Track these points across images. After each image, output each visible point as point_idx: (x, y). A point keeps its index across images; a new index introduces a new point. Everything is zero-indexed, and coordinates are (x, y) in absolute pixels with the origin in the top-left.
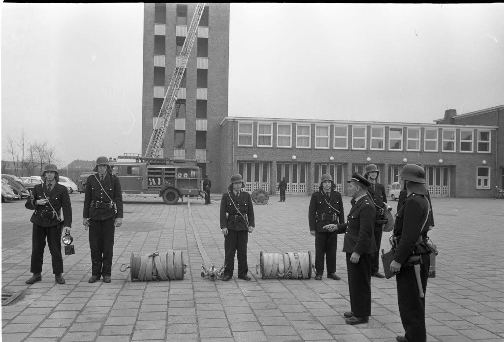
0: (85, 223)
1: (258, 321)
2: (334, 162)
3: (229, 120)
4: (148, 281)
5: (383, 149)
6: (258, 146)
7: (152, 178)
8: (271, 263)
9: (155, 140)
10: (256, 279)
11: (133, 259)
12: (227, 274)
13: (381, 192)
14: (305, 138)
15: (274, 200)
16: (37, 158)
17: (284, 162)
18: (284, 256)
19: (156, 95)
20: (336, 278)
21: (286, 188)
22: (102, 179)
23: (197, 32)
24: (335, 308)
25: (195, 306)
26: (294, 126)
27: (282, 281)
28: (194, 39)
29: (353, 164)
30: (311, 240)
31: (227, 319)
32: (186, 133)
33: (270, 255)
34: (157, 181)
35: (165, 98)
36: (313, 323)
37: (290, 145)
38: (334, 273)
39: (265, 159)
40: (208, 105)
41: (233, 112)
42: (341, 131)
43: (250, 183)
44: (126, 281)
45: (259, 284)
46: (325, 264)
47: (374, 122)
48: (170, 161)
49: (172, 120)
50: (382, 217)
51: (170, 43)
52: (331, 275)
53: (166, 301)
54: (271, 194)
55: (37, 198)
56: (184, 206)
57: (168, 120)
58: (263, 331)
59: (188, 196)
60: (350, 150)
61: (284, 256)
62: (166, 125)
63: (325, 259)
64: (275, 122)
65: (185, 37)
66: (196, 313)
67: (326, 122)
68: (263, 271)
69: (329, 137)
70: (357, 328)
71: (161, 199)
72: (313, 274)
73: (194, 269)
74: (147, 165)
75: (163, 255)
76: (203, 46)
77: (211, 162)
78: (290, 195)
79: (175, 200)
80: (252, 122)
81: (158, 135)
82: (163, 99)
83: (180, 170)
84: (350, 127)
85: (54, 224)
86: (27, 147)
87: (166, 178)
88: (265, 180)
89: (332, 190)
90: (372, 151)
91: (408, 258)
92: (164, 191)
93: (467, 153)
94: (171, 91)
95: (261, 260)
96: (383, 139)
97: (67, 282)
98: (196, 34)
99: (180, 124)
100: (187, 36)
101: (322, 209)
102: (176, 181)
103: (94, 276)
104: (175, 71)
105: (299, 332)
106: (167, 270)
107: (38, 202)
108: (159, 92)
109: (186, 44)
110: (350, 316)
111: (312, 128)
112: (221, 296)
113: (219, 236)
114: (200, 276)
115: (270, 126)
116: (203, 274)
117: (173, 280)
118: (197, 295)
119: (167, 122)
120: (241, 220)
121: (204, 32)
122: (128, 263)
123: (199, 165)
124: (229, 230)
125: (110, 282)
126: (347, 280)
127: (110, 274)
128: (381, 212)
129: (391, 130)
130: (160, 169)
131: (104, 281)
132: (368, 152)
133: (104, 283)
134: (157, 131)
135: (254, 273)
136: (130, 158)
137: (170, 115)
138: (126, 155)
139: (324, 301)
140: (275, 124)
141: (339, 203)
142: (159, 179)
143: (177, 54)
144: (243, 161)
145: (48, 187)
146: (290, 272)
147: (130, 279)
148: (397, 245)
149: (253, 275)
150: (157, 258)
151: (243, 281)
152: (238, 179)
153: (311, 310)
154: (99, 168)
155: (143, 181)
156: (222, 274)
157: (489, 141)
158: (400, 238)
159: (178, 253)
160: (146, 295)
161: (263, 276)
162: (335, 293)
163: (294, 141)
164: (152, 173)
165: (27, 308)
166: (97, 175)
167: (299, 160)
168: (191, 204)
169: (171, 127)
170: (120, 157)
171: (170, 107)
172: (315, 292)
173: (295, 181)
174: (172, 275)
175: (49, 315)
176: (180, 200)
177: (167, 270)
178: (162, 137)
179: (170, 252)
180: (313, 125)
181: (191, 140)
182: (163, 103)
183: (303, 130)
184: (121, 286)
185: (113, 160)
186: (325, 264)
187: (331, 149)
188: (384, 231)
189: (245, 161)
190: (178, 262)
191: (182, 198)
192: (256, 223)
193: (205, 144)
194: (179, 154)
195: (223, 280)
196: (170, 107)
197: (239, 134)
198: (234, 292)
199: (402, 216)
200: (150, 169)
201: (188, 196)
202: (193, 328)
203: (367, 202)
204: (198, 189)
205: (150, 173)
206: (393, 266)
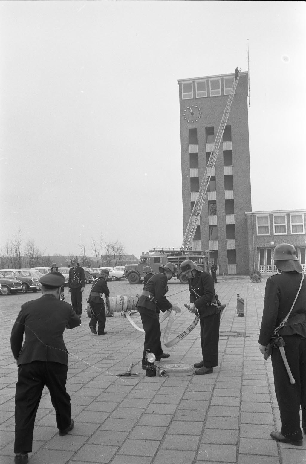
6: (275, 234)
16: (111, 253)
40: (235, 203)
43: (270, 266)
51: (202, 158)
64: (289, 213)
71: (178, 281)
76: (228, 157)
80: (268, 215)
86: (105, 246)
93: (283, 235)
111: (287, 218)
115: (284, 217)
121: (228, 146)
130: (177, 258)
138: (154, 250)
144: (263, 248)
154: (74, 264)
181: (223, 233)
189: (265, 248)
193: (234, 235)
197: (257, 225)
200: (169, 259)
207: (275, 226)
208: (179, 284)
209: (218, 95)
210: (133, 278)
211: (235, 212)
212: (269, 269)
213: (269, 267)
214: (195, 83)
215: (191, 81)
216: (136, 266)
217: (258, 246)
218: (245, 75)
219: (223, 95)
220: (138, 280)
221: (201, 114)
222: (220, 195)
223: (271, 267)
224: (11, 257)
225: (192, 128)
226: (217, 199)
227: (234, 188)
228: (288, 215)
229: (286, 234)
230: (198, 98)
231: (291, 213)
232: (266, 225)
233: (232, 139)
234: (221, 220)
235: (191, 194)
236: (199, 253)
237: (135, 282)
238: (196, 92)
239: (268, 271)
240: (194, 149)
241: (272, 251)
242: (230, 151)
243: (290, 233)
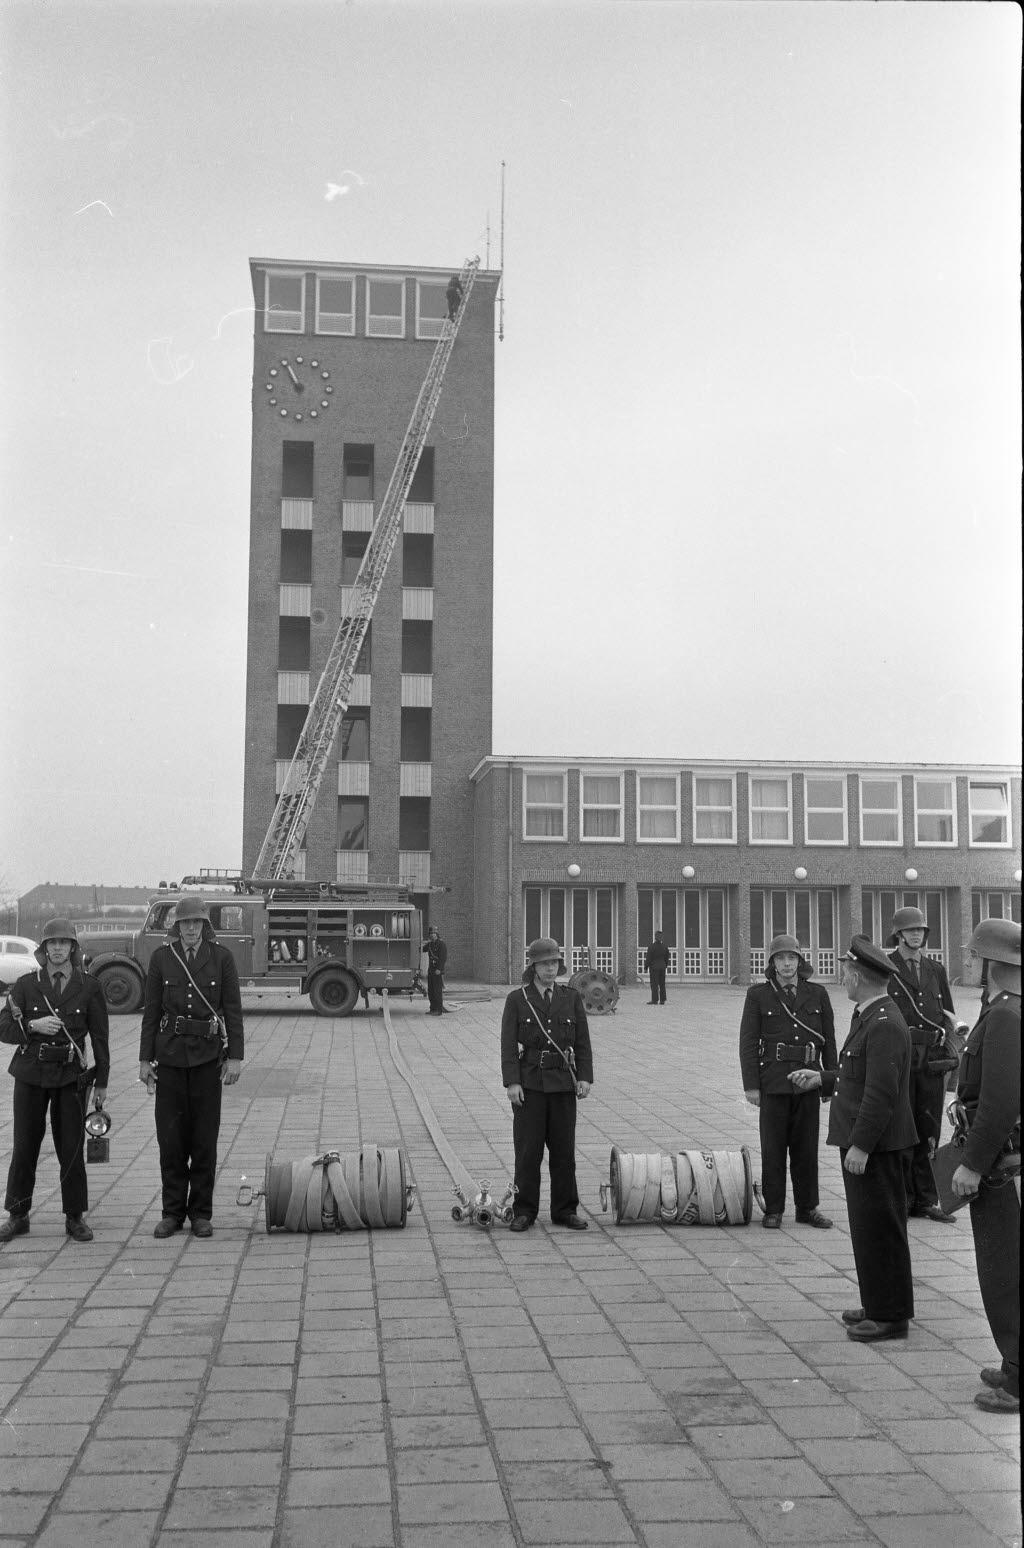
0: (144, 1076)
1: (617, 1333)
2: (807, 882)
3: (495, 766)
4: (312, 1231)
5: (954, 844)
6: (583, 839)
7: (279, 939)
8: (641, 1180)
9: (283, 830)
10: (601, 1226)
11: (271, 1171)
12: (524, 1208)
13: (935, 980)
14: (667, 812)
15: (634, 1000)
17: (658, 887)
18: (675, 1161)
19: (285, 698)
20: (820, 1223)
21: (668, 963)
22: (191, 955)
23: (402, 517)
24: (818, 1301)
25: (446, 1295)
26: (685, 779)
27: (672, 1230)
28: (395, 539)
29: (864, 888)
30: (748, 1114)
31: (534, 1326)
32: (371, 801)
33: (640, 1158)
34: (293, 949)
35: (312, 705)
36: (761, 1339)
37: (787, 838)
38: (813, 1208)
39: (604, 876)
41: (506, 743)
42: (826, 792)
43: (694, 950)
44: (252, 1233)
45: (612, 1239)
46: (789, 1185)
47: (925, 765)
48: (331, 889)
49: (333, 765)
50: (941, 1053)
51: (326, 551)
52: (807, 1214)
53: (368, 1283)
54: (623, 982)
55: (29, 1015)
56: (373, 1019)
57: (322, 767)
58: (630, 1355)
59: (385, 991)
60: (854, 847)
61: (675, 1161)
62: (316, 783)
63: (788, 1171)
65: (369, 534)
66: (452, 1313)
67: (781, 766)
68: (619, 1205)
69: (789, 809)
70: (880, 1351)
71: (305, 1002)
72: (758, 1212)
73: (433, 1201)
74: (267, 901)
75: (350, 1158)
76: (418, 555)
77: (448, 890)
78: (677, 985)
79: (346, 1004)
80: (565, 769)
81: (292, 813)
82: (306, 708)
83: (360, 916)
84: (853, 779)
85: (72, 1077)
87: (321, 940)
88: (604, 940)
89: (802, 979)
90: (920, 849)
91: (999, 1159)
92: (313, 978)
94: (330, 684)
95: (614, 1172)
96: (953, 812)
97: (98, 1236)
98: (401, 525)
99: (354, 779)
100: (374, 531)
101: (776, 1028)
102: (349, 950)
103: (169, 1219)
104: (340, 629)
105: (724, 1358)
106: (363, 1201)
107: (34, 1024)
108: (293, 688)
109: (371, 551)
110: (859, 1321)
112: (511, 1269)
113: (496, 1106)
114: (450, 1218)
116: (456, 1212)
117: (378, 1228)
118: (448, 1267)
119: (319, 776)
120: (557, 1063)
121: (420, 519)
122: (258, 1183)
123: (406, 895)
124: (525, 1090)
125: (209, 1234)
126: (847, 1226)
127: (208, 1214)
128: (939, 1039)
129: (975, 786)
130: (304, 913)
131: (195, 1231)
132: (907, 851)
133: (196, 1238)
134: (288, 800)
135: (596, 1209)
136: (218, 881)
137: (328, 753)
138: (205, 874)
139: (788, 1283)
140: (630, 775)
141: (821, 1014)
142: (300, 943)
143: (346, 579)
145: (53, 982)
146: (694, 1206)
147: (262, 1226)
148: (967, 1127)
149: (592, 1216)
150: (335, 1169)
151: (565, 1230)
152: (549, 951)
153: (754, 1306)
155: (254, 948)
156: (509, 1212)
158: (975, 1107)
159: (391, 1155)
160: (313, 1269)
161: (620, 1216)
162: (823, 1261)
163: (687, 824)
164: (284, 925)
165: (13, 1300)
166: (178, 946)
167: (706, 879)
168: (395, 1014)
169: (329, 785)
170: (187, 880)
171: (324, 731)
172: (761, 1259)
173: (692, 940)
174: (375, 1215)
175: (76, 1317)
176: (360, 1004)
177: (363, 1201)
178: (304, 817)
179: (370, 1151)
180: (742, 777)
181: (387, 824)
182: (307, 722)
183: (713, 791)
184: (242, 1244)
185: (168, 886)
186: (789, 1185)
187: (799, 846)
188: (948, 1090)
189: (546, 885)
190: (393, 1179)
191: (365, 996)
192: (596, 1076)
193: (426, 837)
194: (352, 868)
195: (513, 1229)
196: (324, 731)
197: (526, 805)
198: (543, 1259)
199: (979, 1053)
200: (272, 913)
201: (385, 991)
202: (450, 1349)
203: (883, 1014)
204: (415, 970)
205: (273, 926)
206: (960, 1181)
209: (345, 334)
210: (115, 987)
211: (435, 754)
212: (604, 962)
213: (693, 956)
214: (314, 282)
215: (352, 276)
216: (128, 939)
218: (491, 281)
219: (410, 339)
221: (329, 393)
223: (698, 955)
225: (295, 437)
226: (371, 702)
227: (435, 667)
228: (630, 775)
230: (271, 333)
231: (638, 770)
232: (557, 805)
234: (384, 778)
235: (280, 676)
237: (123, 1006)
238: (417, 317)
239: (687, 971)
241: (703, 900)
242: (429, 538)
243: (578, 836)
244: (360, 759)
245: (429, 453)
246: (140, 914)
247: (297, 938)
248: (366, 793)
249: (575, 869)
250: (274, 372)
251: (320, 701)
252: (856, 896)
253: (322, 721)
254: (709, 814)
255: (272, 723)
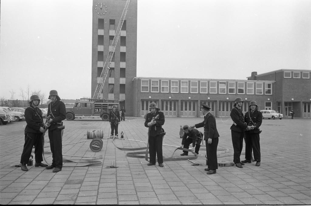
6: (152, 92)
7: (96, 108)
9: (98, 90)
14: (176, 87)
17: (165, 100)
43: (171, 111)
49: (107, 78)
51: (106, 39)
57: (105, 79)
60: (199, 93)
62: (104, 82)
67: (186, 79)
71: (101, 119)
74: (94, 102)
81: (100, 87)
83: (110, 105)
99: (111, 81)
102: (108, 110)
108: (100, 64)
115: (177, 82)
121: (123, 33)
129: (220, 83)
130: (101, 104)
132: (208, 94)
138: (84, 98)
142: (100, 109)
143: (110, 44)
157: (271, 89)
163: (199, 90)
169: (107, 82)
170: (81, 99)
180: (180, 81)
181: (117, 89)
183: (174, 84)
189: (145, 100)
194: (111, 97)
196: (106, 72)
197: (141, 86)
205: (95, 106)
207: (152, 87)
208: (78, 121)
211: (126, 76)
216: (71, 109)
217: (141, 98)
220: (72, 118)
222: (117, 64)
224: (26, 101)
229: (158, 92)
232: (177, 87)
233: (127, 29)
234: (117, 80)
236: (113, 101)
240: (101, 32)
244: (113, 77)
245: (125, 21)
246: (72, 105)
247: (99, 108)
248: (114, 83)
249: (150, 97)
250: (96, 6)
251: (105, 67)
252: (199, 102)
253: (105, 71)
254: (174, 88)
255: (96, 70)
